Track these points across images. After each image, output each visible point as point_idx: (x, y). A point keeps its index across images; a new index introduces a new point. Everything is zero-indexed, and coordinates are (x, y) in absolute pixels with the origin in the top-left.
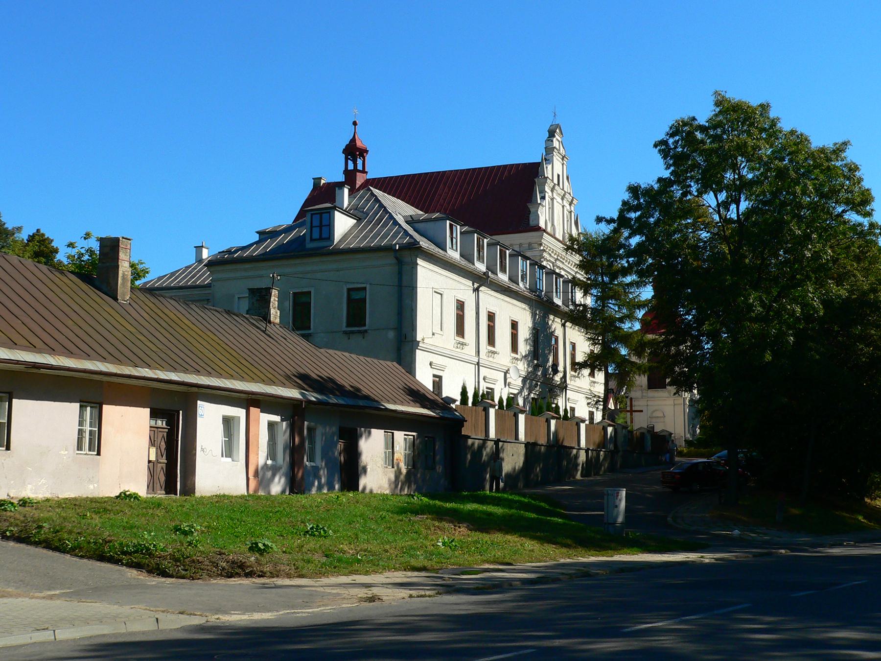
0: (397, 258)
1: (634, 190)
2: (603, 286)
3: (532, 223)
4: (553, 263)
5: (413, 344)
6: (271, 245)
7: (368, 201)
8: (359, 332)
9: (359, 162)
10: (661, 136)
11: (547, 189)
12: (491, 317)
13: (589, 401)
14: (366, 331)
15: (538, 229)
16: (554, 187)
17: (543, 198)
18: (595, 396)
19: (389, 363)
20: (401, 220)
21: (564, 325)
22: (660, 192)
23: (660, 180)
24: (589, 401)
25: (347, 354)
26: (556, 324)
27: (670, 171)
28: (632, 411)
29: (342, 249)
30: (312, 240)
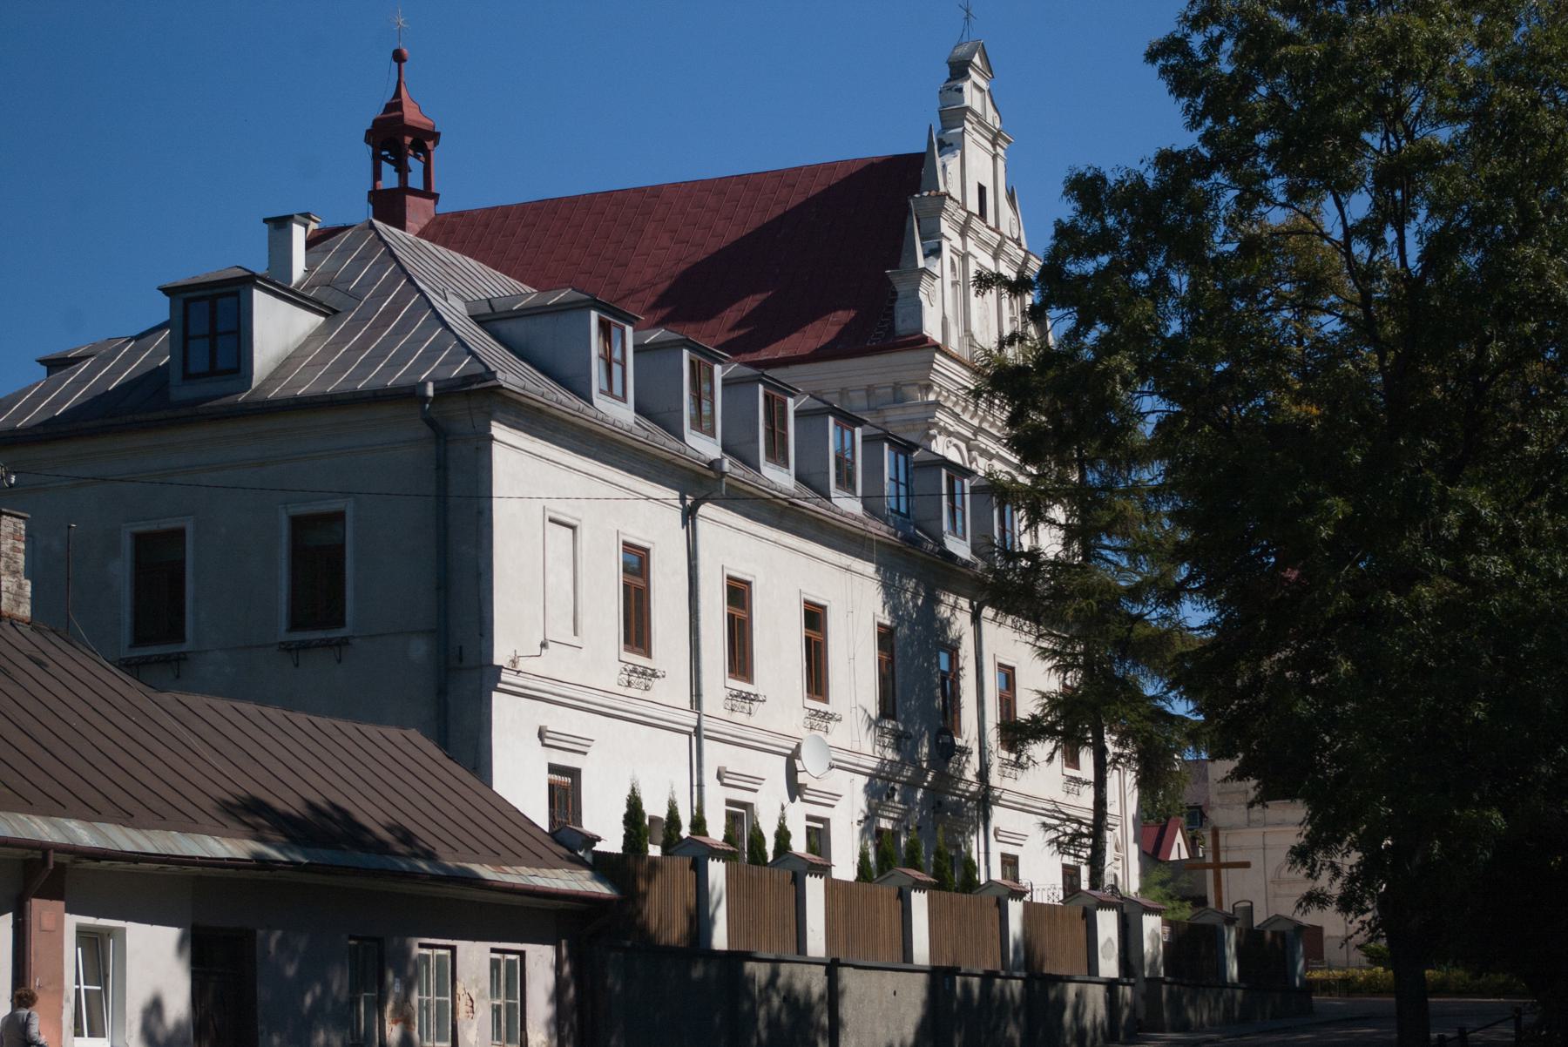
0: (431, 423)
1: (1086, 189)
2: (1081, 499)
3: (902, 326)
4: (966, 440)
5: (486, 676)
6: (73, 392)
7: (362, 260)
8: (327, 644)
9: (415, 164)
10: (1166, 25)
11: (945, 227)
12: (738, 593)
13: (1053, 834)
14: (344, 642)
15: (920, 342)
16: (967, 222)
17: (936, 252)
18: (1070, 819)
19: (394, 733)
20: (455, 311)
21: (976, 618)
22: (1162, 192)
23: (1165, 159)
24: (1053, 834)
25: (249, 708)
26: (957, 614)
27: (1201, 131)
28: (1218, 866)
29: (272, 401)
30: (187, 376)
